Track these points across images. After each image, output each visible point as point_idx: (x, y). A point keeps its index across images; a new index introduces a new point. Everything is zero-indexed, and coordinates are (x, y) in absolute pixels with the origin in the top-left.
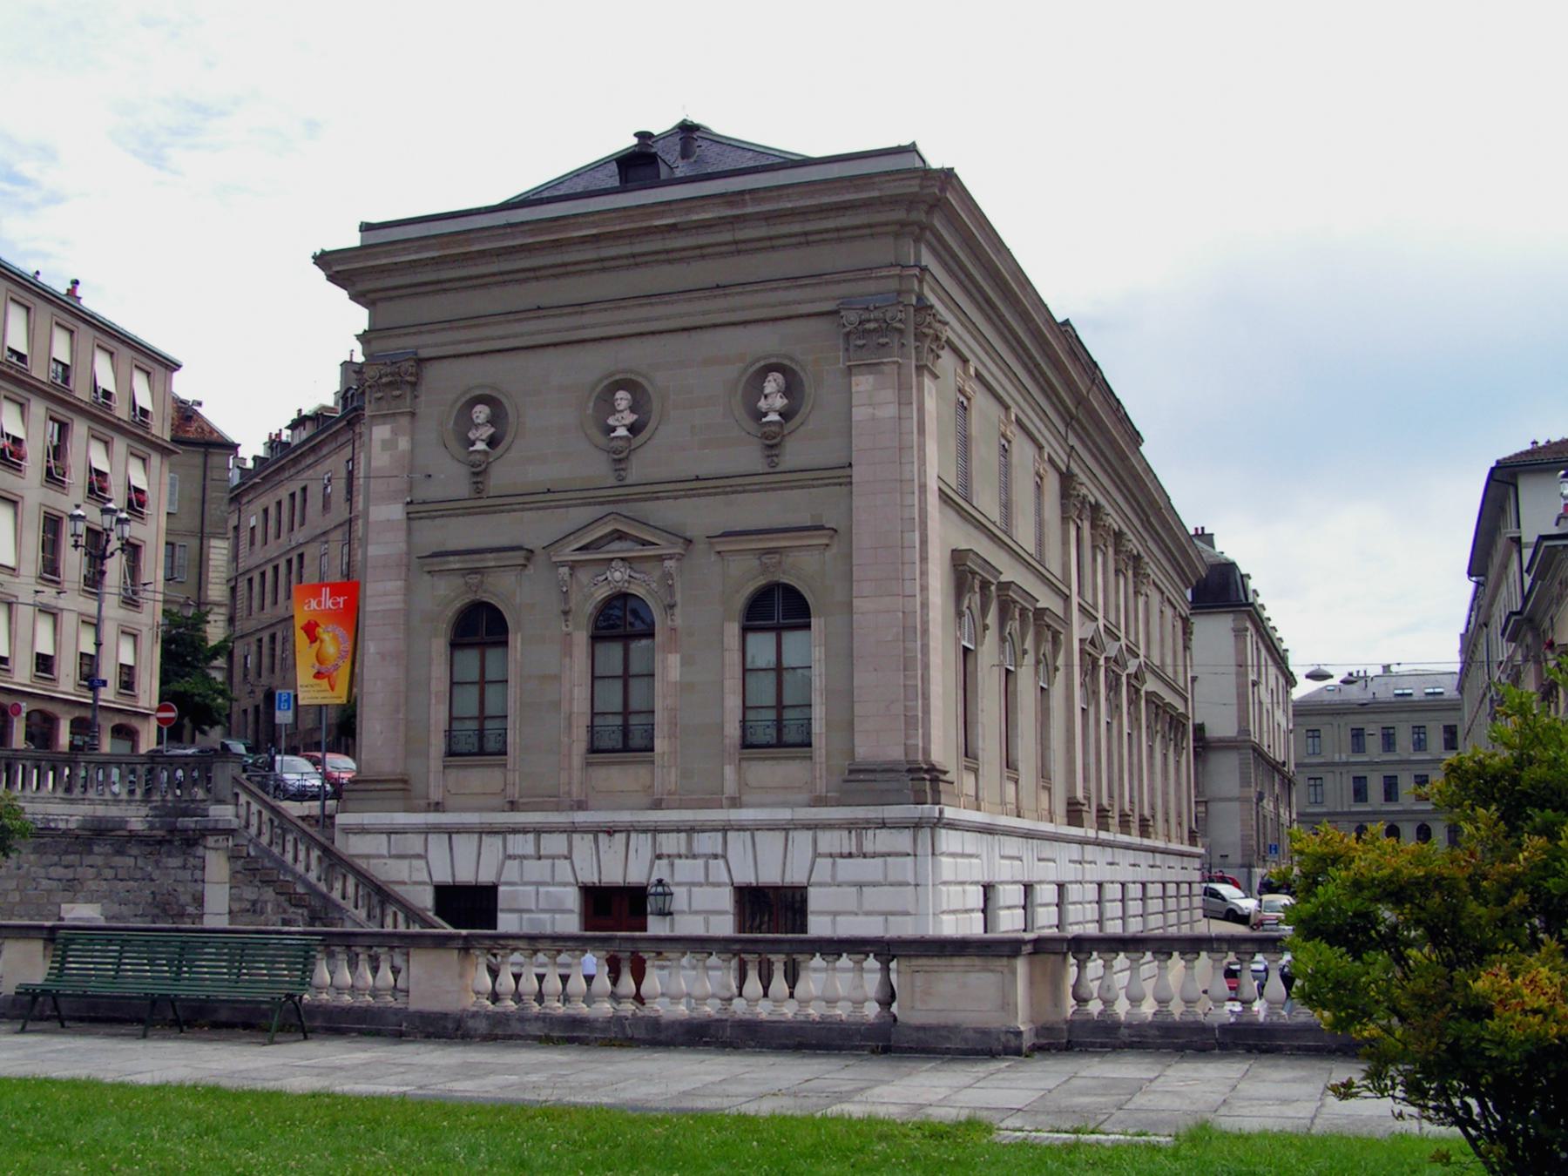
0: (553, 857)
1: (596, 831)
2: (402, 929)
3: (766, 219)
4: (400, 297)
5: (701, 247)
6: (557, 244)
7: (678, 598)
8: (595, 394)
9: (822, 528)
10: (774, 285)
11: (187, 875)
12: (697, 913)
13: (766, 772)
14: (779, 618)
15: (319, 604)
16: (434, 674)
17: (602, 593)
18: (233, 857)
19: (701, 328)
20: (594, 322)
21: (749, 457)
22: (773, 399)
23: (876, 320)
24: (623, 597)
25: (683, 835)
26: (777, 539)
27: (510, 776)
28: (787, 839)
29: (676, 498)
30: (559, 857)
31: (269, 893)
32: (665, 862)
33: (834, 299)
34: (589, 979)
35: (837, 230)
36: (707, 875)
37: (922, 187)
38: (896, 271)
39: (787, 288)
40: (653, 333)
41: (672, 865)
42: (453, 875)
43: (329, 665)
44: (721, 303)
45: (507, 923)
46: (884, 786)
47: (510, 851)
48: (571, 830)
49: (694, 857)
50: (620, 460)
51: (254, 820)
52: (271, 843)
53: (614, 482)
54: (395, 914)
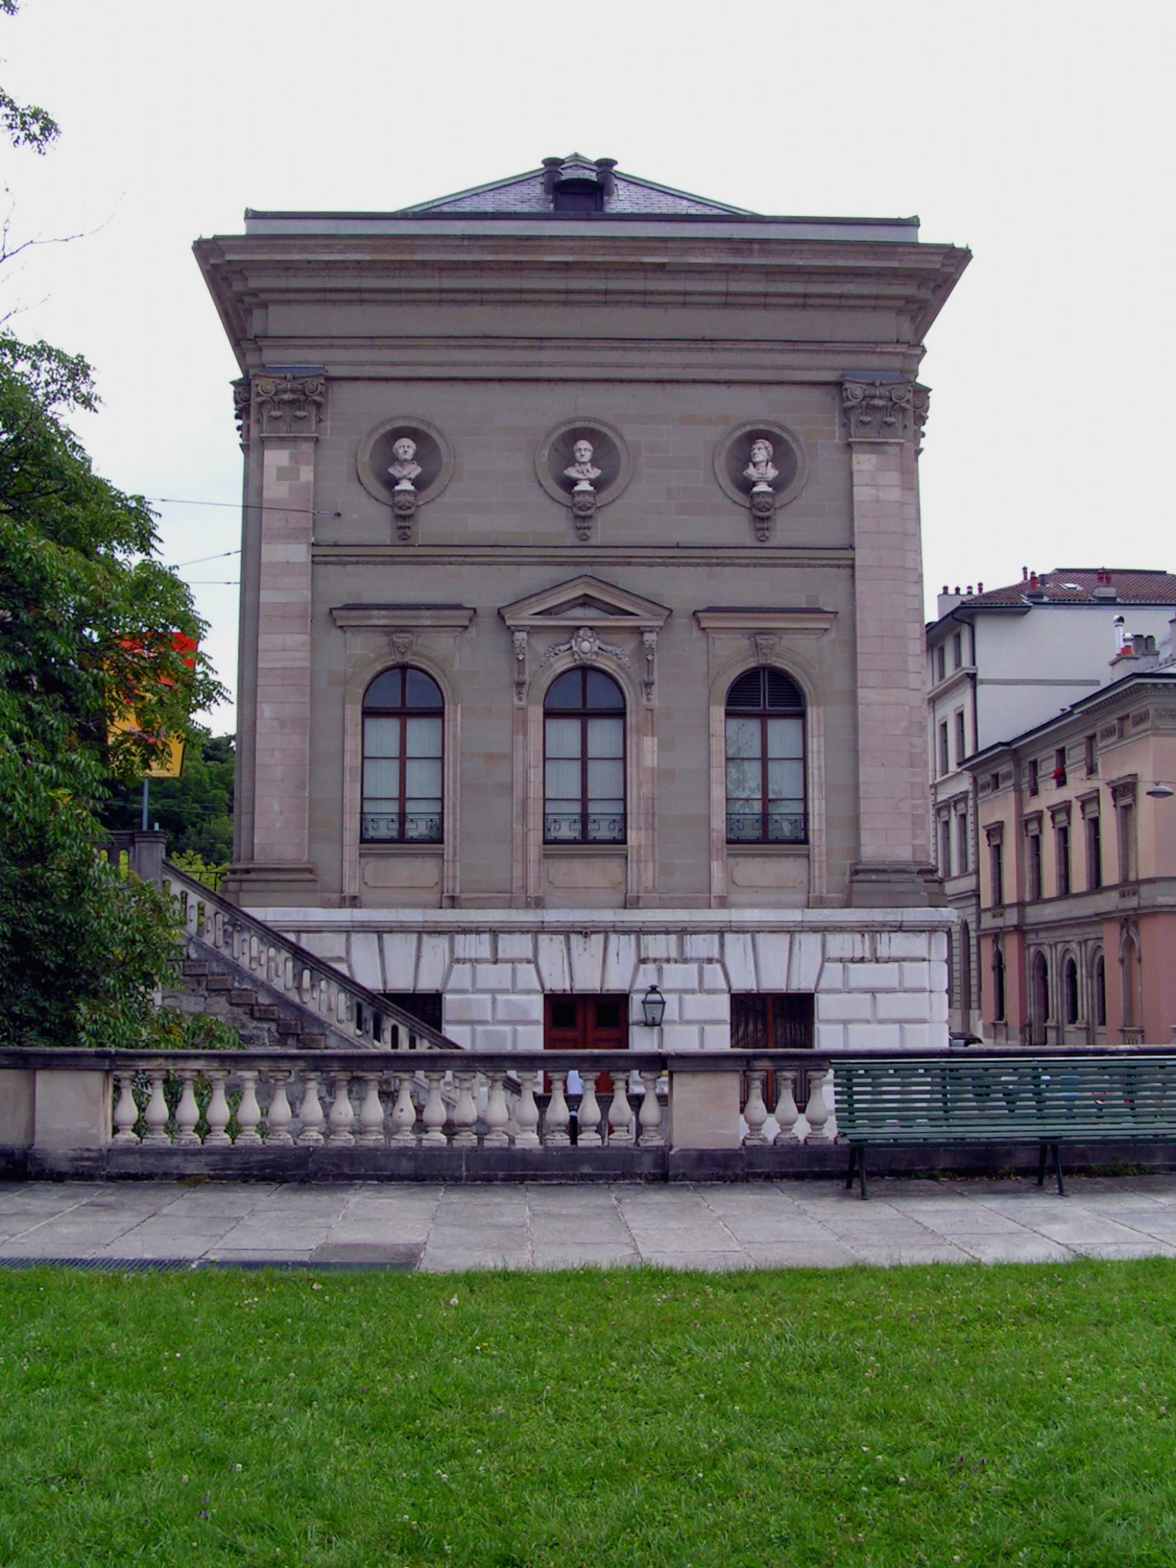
0: (512, 961)
1: (567, 931)
2: (404, 1047)
3: (767, 273)
4: (302, 302)
5: (686, 294)
6: (518, 267)
7: (655, 676)
9: (819, 611)
10: (767, 346)
12: (689, 1022)
14: (764, 705)
16: (347, 747)
17: (563, 663)
19: (678, 382)
20: (551, 361)
21: (733, 527)
22: (763, 470)
23: (881, 398)
24: (585, 669)
25: (673, 937)
27: (449, 869)
28: (791, 943)
29: (651, 565)
30: (520, 961)
32: (651, 967)
35: (840, 296)
37: (943, 265)
38: (901, 349)
39: (781, 351)
40: (622, 381)
41: (660, 970)
42: (385, 982)
44: (709, 358)
46: (901, 888)
47: (460, 952)
48: (538, 930)
49: (685, 961)
50: (582, 517)
53: (577, 542)
54: (395, 1030)
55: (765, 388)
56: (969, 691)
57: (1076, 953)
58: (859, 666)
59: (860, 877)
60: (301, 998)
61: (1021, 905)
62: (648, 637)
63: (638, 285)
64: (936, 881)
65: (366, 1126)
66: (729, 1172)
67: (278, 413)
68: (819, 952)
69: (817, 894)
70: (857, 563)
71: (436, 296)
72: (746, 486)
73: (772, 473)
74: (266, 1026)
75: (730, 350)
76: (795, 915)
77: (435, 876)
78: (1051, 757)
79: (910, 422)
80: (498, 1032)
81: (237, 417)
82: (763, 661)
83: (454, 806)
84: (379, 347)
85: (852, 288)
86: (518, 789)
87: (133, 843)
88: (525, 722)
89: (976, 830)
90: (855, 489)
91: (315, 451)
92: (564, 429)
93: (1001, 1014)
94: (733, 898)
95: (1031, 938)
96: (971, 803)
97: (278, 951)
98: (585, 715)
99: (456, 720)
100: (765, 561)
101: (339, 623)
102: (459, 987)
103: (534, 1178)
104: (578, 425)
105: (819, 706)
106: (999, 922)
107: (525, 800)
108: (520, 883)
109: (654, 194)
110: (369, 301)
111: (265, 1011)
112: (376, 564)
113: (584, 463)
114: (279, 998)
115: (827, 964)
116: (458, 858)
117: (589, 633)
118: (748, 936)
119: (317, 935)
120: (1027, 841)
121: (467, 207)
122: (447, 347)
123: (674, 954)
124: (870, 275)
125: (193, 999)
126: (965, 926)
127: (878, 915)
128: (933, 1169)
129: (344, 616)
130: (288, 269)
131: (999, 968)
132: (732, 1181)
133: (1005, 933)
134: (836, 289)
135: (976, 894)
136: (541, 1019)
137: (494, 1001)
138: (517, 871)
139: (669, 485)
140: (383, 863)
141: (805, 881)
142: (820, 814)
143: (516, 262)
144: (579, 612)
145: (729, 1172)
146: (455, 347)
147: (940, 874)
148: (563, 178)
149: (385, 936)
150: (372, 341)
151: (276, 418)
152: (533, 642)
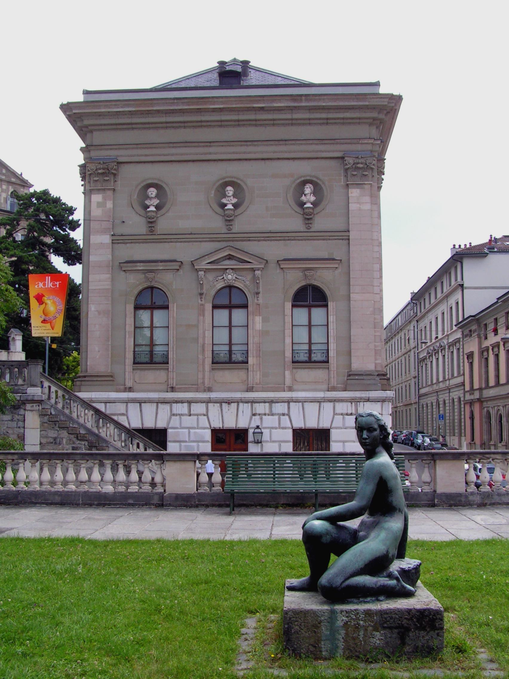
0: (197, 415)
1: (221, 402)
5: (274, 120)
6: (199, 111)
7: (261, 290)
8: (215, 187)
9: (334, 259)
10: (311, 142)
11: (14, 424)
13: (306, 374)
14: (310, 301)
15: (44, 285)
16: (127, 323)
18: (42, 415)
20: (216, 152)
21: (296, 223)
22: (309, 197)
23: (362, 163)
24: (230, 287)
25: (267, 404)
26: (313, 264)
27: (171, 375)
28: (320, 407)
29: (259, 241)
30: (201, 415)
31: (64, 434)
32: (257, 417)
33: (341, 151)
34: (210, 475)
35: (343, 119)
36: (279, 424)
37: (389, 103)
38: (371, 141)
39: (317, 144)
40: (246, 160)
41: (261, 419)
42: (143, 424)
43: (51, 316)
45: (172, 448)
46: (369, 382)
47: (174, 412)
48: (208, 401)
50: (229, 220)
51: (53, 395)
52: (63, 408)
53: (227, 231)
55: (309, 161)
56: (460, 293)
57: (502, 411)
58: (351, 284)
59: (351, 377)
60: (99, 431)
61: (480, 389)
62: (258, 273)
63: (252, 117)
64: (385, 379)
65: (56, 482)
66: (189, 503)
67: (97, 179)
68: (332, 412)
69: (332, 385)
70: (351, 238)
71: (165, 125)
72: (302, 204)
73: (313, 198)
74: (83, 443)
75: (294, 144)
76: (321, 395)
77: (165, 378)
78: (492, 322)
79: (375, 174)
80: (190, 446)
81: (82, 180)
82: (308, 282)
83: (173, 348)
84: (140, 148)
85: (348, 115)
86: (201, 340)
87: (28, 365)
88: (203, 310)
89: (463, 355)
90: (350, 204)
91: (114, 194)
92: (221, 182)
93: (473, 439)
94: (295, 387)
95: (485, 404)
96: (461, 343)
97: (89, 411)
98: (230, 307)
99: (174, 310)
100: (315, 238)
101: (123, 269)
102: (174, 426)
103: (109, 505)
104: (227, 180)
105: (333, 302)
106: (472, 397)
107: (203, 346)
108: (202, 381)
109: (266, 75)
110: (136, 128)
111: (83, 437)
112: (139, 243)
113: (230, 196)
114: (89, 431)
115: (335, 416)
116: (174, 370)
117: (231, 271)
118: (301, 404)
119: (114, 404)
120: (483, 360)
121: (183, 85)
122: (170, 147)
123: (267, 412)
124: (356, 109)
125: (53, 431)
126: (460, 398)
127: (358, 394)
128: (278, 504)
129: (127, 265)
130: (100, 115)
131: (472, 418)
132: (190, 507)
133: (474, 402)
134: (341, 115)
135: (463, 384)
136: (210, 440)
137: (189, 432)
138: (200, 376)
139: (268, 206)
140: (143, 373)
141: (327, 380)
142: (334, 350)
143: (198, 109)
144: (227, 262)
145: (189, 503)
146: (173, 147)
147: (388, 376)
148: (227, 69)
149: (143, 404)
150: (138, 145)
151: (96, 181)
152: (207, 275)
